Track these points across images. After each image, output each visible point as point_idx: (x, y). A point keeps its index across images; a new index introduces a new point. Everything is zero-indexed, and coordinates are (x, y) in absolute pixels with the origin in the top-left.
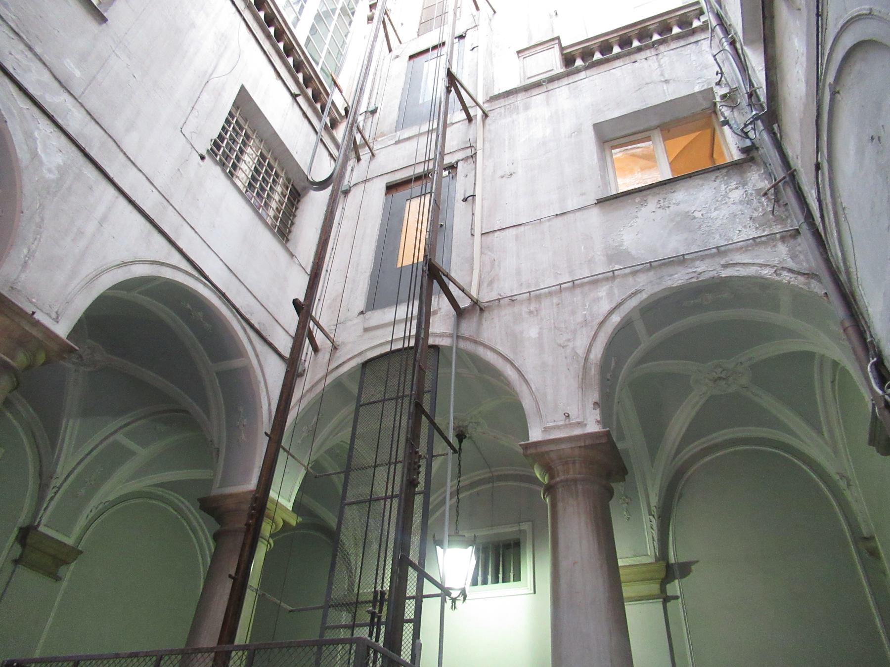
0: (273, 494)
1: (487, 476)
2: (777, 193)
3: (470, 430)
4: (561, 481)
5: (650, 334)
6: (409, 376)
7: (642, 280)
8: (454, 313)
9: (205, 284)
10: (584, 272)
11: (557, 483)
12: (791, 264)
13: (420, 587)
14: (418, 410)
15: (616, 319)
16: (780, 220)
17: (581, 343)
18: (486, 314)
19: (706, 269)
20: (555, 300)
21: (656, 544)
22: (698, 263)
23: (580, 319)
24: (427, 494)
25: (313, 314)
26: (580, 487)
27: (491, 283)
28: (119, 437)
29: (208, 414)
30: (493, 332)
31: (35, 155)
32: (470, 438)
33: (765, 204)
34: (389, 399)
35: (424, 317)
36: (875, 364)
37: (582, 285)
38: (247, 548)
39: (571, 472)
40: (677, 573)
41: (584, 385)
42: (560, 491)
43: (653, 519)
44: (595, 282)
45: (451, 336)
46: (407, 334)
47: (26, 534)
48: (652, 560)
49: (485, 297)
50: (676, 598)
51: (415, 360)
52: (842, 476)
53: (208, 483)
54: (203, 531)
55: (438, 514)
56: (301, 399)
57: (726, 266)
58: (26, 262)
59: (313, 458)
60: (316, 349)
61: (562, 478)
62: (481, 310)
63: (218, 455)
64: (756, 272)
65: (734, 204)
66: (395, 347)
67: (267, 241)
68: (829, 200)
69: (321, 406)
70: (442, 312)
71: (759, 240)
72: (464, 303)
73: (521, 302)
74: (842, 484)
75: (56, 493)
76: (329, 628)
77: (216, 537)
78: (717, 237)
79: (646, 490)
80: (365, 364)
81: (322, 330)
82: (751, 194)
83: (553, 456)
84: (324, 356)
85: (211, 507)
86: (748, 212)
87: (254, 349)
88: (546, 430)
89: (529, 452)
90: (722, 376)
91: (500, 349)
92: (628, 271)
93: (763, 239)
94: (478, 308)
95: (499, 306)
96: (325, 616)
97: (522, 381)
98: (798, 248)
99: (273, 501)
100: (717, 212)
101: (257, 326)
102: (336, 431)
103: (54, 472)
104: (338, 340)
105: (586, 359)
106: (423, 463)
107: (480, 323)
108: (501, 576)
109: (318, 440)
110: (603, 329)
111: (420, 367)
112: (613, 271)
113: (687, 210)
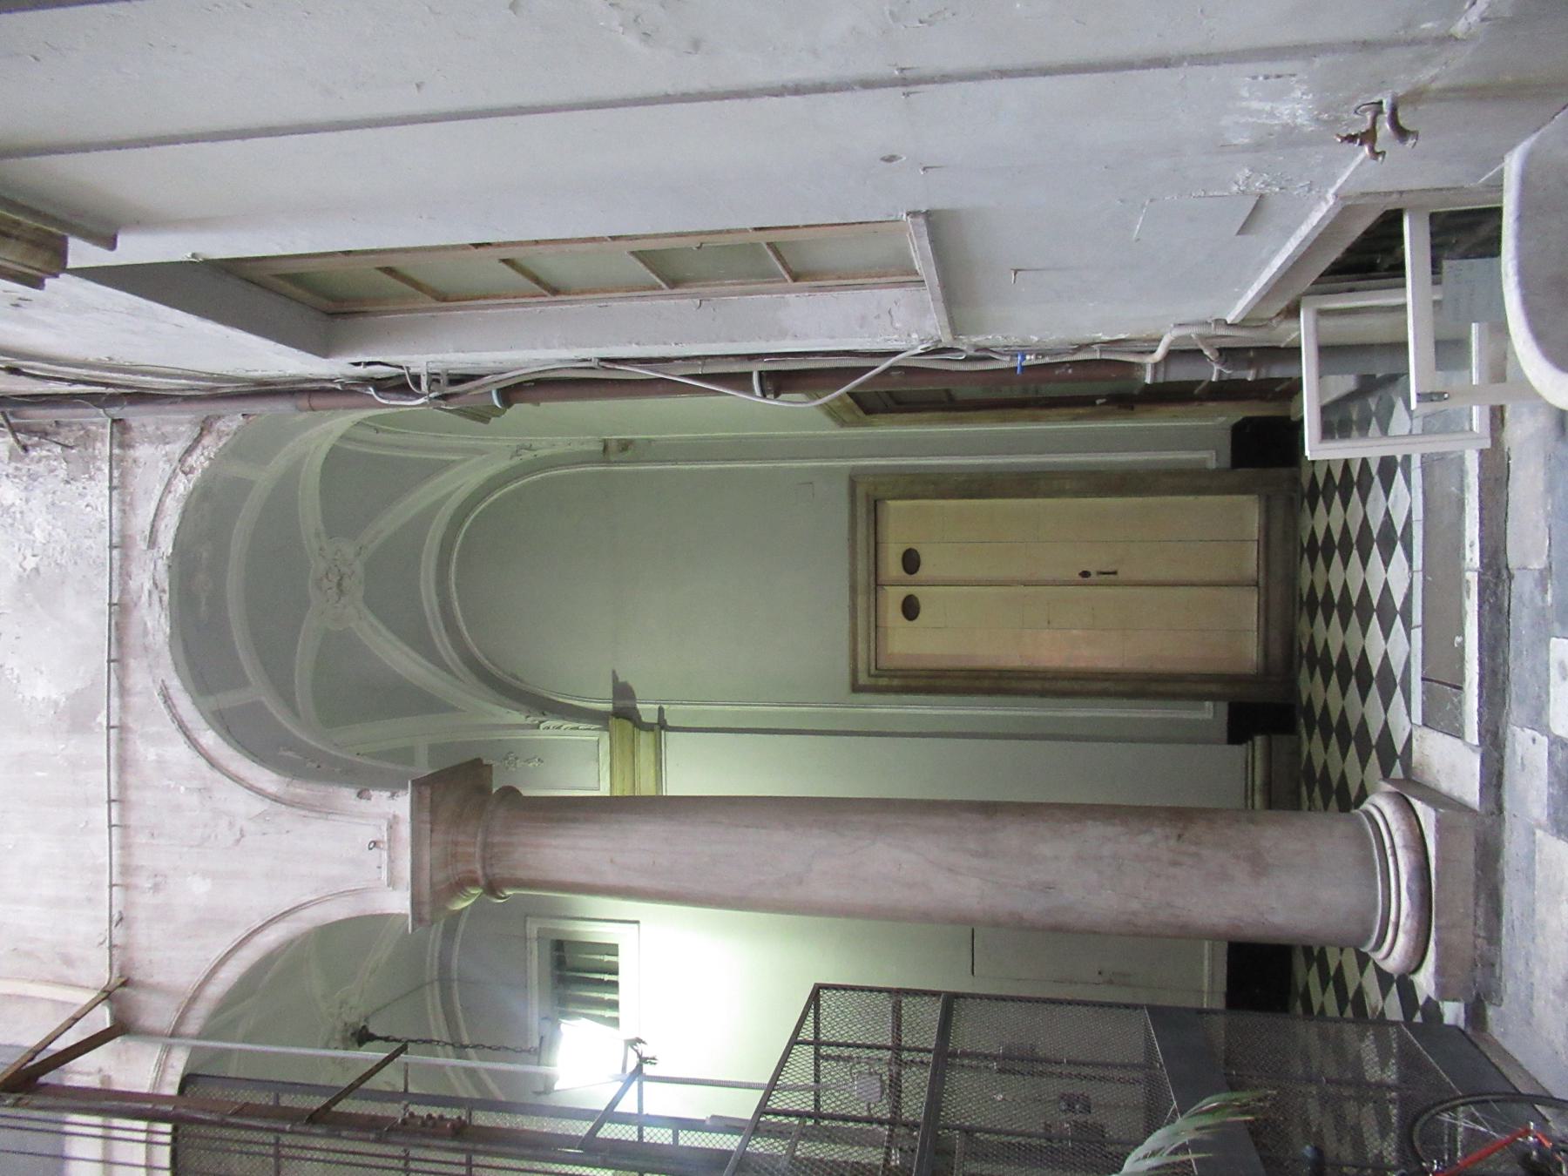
1: (437, 992)
2: (29, 431)
4: (484, 868)
5: (246, 683)
7: (141, 678)
8: (118, 1040)
10: (98, 781)
11: (485, 875)
12: (177, 448)
13: (625, 1119)
15: (209, 738)
16: (87, 439)
17: (242, 804)
18: (137, 976)
19: (149, 574)
20: (141, 839)
21: (582, 726)
22: (133, 584)
23: (194, 799)
26: (496, 839)
27: (68, 961)
32: (366, 1020)
33: (44, 453)
35: (108, 1103)
36: (377, 390)
37: (123, 786)
39: (471, 850)
40: (628, 703)
42: (499, 871)
43: (547, 724)
44: (122, 763)
45: (168, 1049)
48: (606, 735)
49: (101, 975)
50: (661, 710)
51: (224, 1124)
52: (517, 453)
55: (492, 1086)
57: (152, 542)
62: (124, 984)
64: (178, 501)
65: (27, 501)
68: (84, 372)
71: (115, 482)
72: (102, 1018)
73: (128, 904)
74: (528, 456)
78: (88, 542)
79: (497, 727)
82: (17, 469)
83: (440, 876)
86: (51, 483)
88: (392, 882)
89: (427, 917)
90: (335, 580)
91: (220, 951)
92: (115, 702)
93: (116, 474)
98: (150, 429)
100: (37, 532)
105: (276, 799)
106: (421, 1111)
108: (607, 977)
110: (223, 762)
112: (109, 727)
113: (15, 579)
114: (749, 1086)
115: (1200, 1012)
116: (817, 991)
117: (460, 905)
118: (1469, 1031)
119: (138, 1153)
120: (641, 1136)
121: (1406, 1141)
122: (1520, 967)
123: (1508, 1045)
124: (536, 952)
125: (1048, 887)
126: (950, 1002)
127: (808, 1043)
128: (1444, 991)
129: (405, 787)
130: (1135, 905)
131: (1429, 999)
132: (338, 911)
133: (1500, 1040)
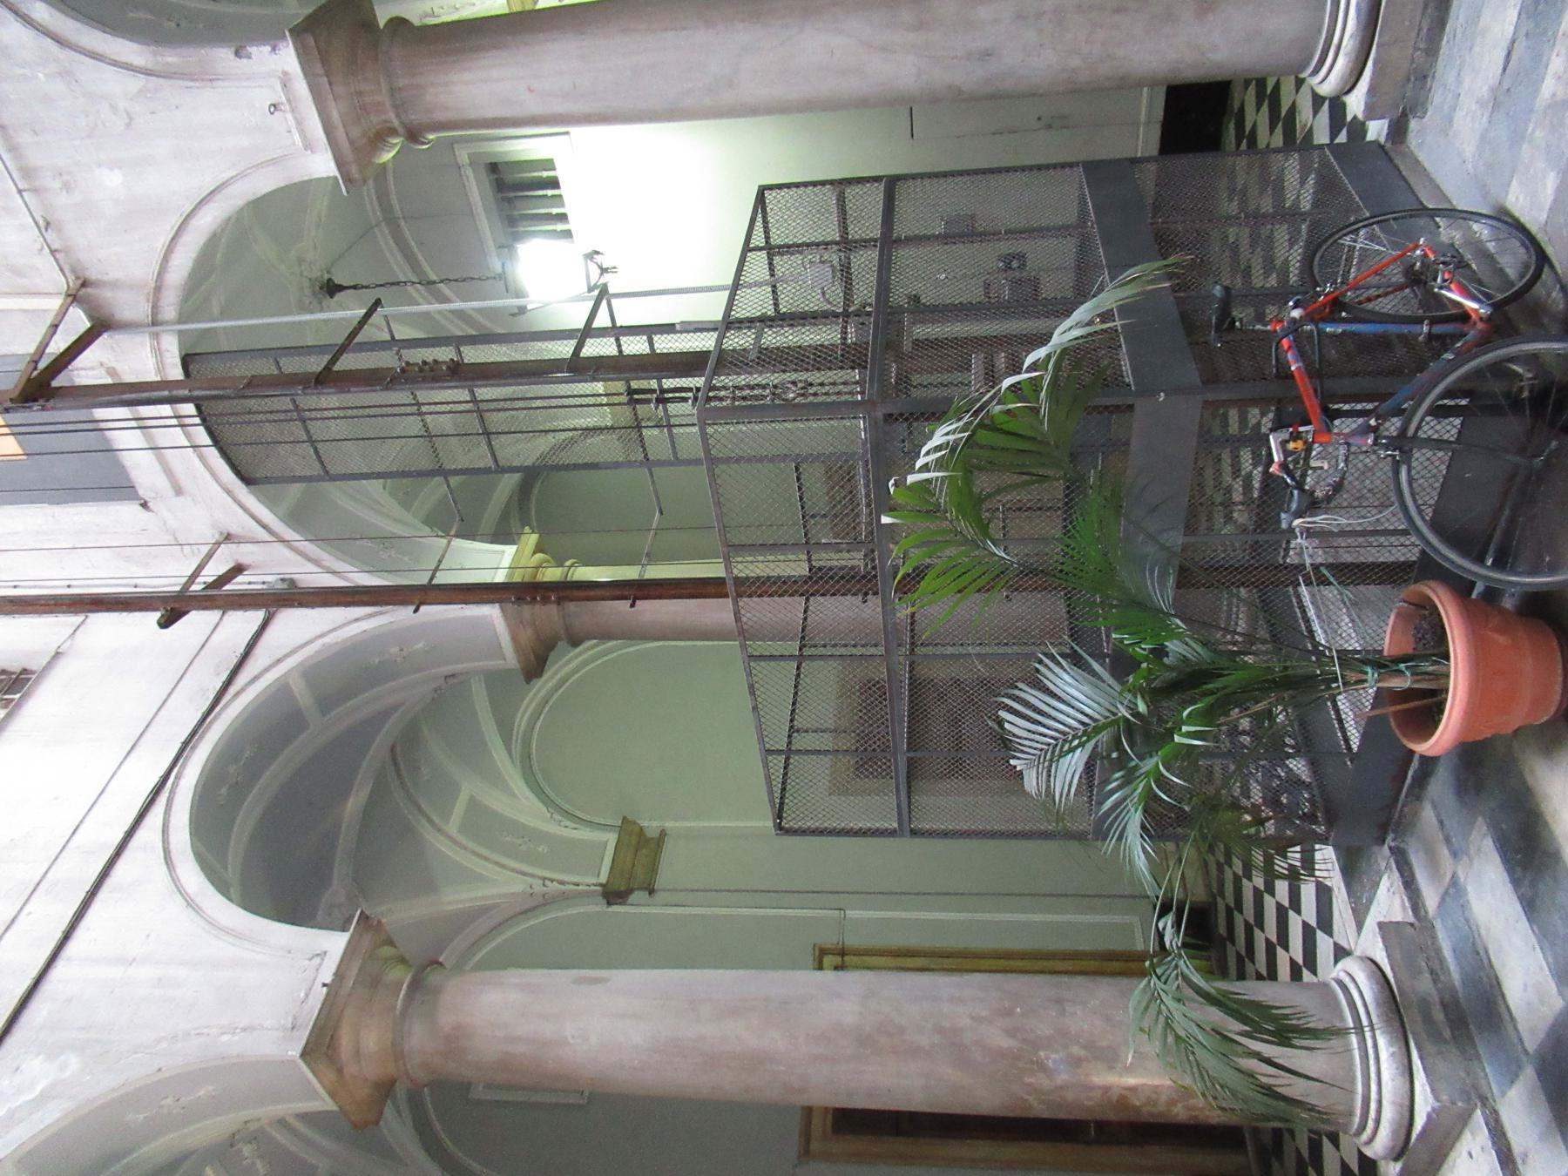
0: (500, 577)
3: (316, 274)
4: (398, 116)
6: (242, 401)
8: (105, 336)
9: (178, 777)
13: (603, 332)
14: (325, 379)
18: (93, 275)
20: (25, 138)
24: (458, 342)
25: (178, 588)
26: (401, 82)
27: (16, 271)
28: (452, 828)
29: (395, 708)
30: (130, 260)
31: (44, 1098)
34: (308, 432)
38: (592, 593)
41: (205, 76)
42: (415, 117)
45: (156, 336)
46: (174, 422)
47: (613, 895)
53: (496, 681)
54: (566, 665)
56: (334, 573)
58: (244, 1030)
59: (427, 530)
60: (238, 569)
61: (392, 115)
62: (84, 284)
63: (453, 676)
66: (205, 439)
67: (41, 706)
69: (341, 538)
70: (109, 358)
72: (78, 321)
75: (552, 881)
76: (675, 454)
77: (575, 643)
80: (248, 481)
81: (200, 568)
83: (356, 132)
84: (245, 553)
85: (534, 667)
87: (266, 670)
88: (309, 146)
94: (81, 292)
95: (66, 250)
96: (660, 463)
97: (219, 197)
99: (510, 575)
101: (224, 677)
102: (374, 506)
103: (524, 893)
104: (212, 536)
107: (115, 285)
109: (399, 530)
111: (248, 385)
114: (710, 289)
115: (1134, 161)
116: (760, 200)
117: (387, 156)
118: (1388, 145)
119: (178, 437)
120: (620, 351)
121: (1308, 261)
122: (1451, 78)
123: (1421, 157)
124: (472, 178)
125: (987, 54)
126: (891, 184)
127: (760, 249)
128: (1372, 111)
129: (283, 37)
130: (1075, 62)
131: (1355, 117)
132: (264, 183)
133: (1416, 152)
